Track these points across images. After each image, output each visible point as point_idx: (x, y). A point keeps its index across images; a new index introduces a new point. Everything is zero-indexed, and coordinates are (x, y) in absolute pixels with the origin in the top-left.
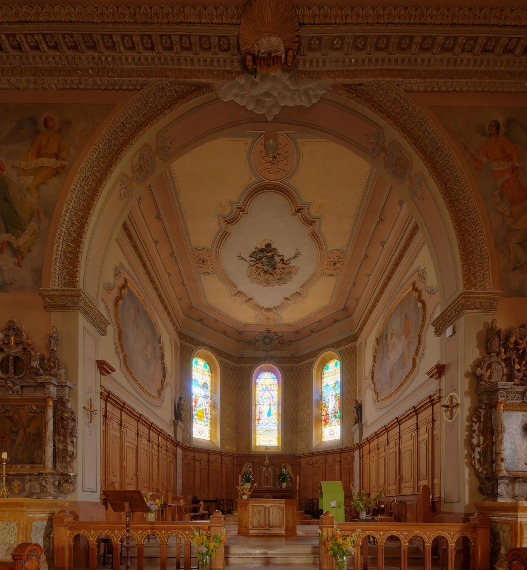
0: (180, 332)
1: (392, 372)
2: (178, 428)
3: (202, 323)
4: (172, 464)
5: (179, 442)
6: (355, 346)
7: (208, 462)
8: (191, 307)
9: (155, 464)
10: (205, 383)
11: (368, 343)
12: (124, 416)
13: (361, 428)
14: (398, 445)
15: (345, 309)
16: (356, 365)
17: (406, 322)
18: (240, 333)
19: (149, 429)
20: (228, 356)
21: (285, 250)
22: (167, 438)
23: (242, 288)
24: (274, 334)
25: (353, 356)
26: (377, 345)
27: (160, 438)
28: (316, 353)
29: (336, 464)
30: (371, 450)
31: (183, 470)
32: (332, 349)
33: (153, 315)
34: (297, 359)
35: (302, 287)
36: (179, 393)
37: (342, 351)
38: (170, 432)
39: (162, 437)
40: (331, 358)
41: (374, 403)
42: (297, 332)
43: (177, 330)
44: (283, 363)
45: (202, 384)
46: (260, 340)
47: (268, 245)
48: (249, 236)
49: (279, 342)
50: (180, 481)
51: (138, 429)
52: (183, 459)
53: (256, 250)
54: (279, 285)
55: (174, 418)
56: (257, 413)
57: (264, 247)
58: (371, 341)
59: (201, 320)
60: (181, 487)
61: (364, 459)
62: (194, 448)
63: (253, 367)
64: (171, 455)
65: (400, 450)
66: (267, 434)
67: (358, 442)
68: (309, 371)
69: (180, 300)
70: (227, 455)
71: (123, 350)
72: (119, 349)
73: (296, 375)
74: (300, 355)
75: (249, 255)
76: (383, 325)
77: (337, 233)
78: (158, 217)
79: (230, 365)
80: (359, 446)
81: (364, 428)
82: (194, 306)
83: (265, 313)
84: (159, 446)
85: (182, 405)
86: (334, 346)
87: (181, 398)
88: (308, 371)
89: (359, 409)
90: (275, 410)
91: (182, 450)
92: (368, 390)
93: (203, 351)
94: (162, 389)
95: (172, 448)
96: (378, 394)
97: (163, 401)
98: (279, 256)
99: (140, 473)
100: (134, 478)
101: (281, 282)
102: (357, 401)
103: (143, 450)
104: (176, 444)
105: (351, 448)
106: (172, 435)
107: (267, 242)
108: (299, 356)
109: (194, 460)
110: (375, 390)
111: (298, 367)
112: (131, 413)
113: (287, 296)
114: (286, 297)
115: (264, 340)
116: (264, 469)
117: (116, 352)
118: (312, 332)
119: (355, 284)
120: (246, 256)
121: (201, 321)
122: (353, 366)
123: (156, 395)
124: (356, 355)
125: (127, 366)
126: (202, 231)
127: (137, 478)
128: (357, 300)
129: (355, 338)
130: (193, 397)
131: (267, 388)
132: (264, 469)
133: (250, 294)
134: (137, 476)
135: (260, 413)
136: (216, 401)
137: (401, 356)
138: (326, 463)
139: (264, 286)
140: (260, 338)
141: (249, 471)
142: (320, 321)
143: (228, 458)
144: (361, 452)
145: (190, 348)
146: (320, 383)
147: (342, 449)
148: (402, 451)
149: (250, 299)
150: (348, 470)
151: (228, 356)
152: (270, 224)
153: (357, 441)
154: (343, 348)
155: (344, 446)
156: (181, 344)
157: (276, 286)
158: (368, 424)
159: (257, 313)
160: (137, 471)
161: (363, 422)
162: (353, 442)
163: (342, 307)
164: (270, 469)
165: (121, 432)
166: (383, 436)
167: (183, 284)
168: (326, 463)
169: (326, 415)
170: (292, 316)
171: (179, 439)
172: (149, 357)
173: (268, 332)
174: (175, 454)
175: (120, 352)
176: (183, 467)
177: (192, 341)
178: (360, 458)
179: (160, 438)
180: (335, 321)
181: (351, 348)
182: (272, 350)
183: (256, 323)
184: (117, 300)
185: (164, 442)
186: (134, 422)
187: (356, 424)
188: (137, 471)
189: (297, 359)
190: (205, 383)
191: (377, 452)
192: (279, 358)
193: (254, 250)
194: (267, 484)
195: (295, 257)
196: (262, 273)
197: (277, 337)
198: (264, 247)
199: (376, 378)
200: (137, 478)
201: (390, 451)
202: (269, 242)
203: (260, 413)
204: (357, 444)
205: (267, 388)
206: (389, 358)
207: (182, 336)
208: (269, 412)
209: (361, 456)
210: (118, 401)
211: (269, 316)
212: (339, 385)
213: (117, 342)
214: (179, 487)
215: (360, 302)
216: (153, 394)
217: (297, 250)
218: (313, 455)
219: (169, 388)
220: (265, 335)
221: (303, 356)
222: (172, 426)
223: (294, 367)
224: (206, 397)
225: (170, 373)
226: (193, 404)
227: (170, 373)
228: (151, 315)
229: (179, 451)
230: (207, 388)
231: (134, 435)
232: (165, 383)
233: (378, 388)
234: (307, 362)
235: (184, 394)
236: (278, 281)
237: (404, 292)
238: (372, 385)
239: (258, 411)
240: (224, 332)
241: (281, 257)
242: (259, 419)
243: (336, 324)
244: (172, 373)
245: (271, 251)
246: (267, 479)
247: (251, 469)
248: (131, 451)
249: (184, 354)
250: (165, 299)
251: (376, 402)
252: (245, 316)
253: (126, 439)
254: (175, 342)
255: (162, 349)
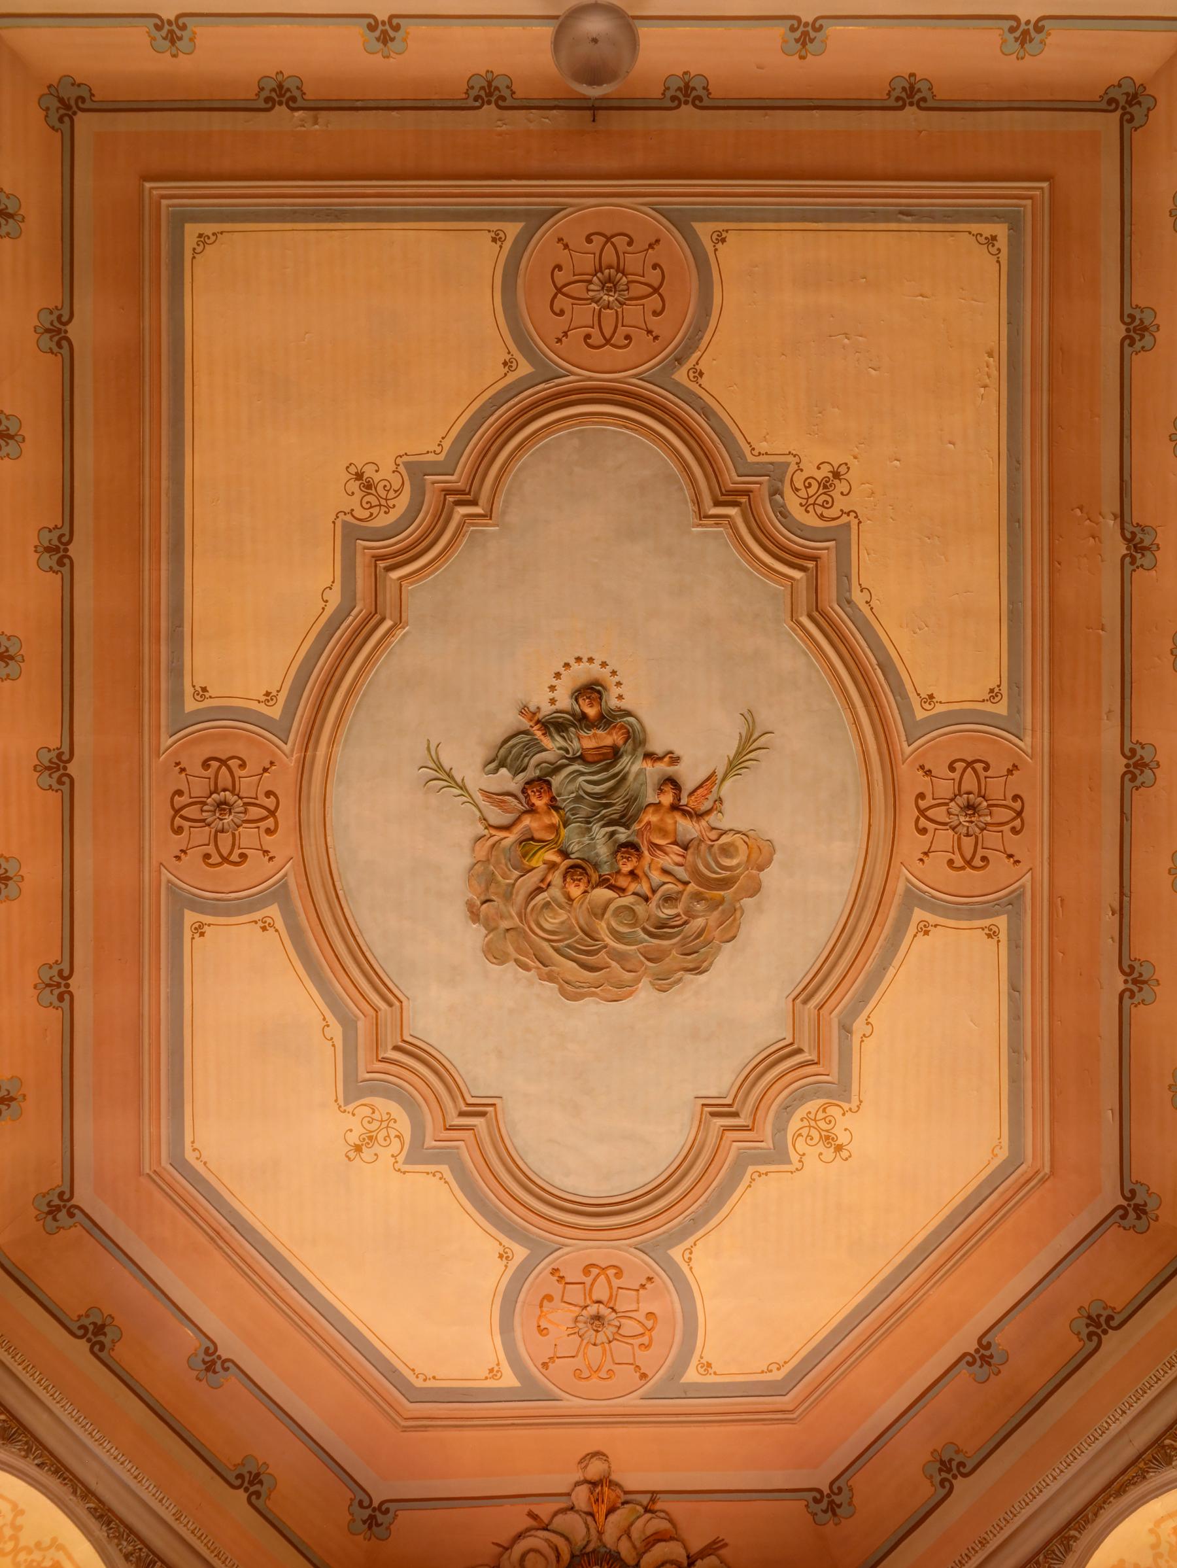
8: (60, 1207)
21: (687, 728)
24: (645, 1526)
47: (591, 690)
48: (486, 656)
53: (526, 724)
57: (564, 701)
75: (479, 759)
77: (943, 612)
78: (58, 552)
98: (649, 756)
107: (582, 673)
113: (719, 1082)
120: (467, 761)
126: (247, 626)
142: (983, 1355)
152: (596, 591)
180: (1099, 1325)
193: (510, 720)
195: (735, 765)
196: (556, 877)
198: (564, 701)
202: (595, 671)
217: (749, 718)
240: (251, 1482)
241: (663, 767)
243: (1111, 1340)
245: (606, 720)
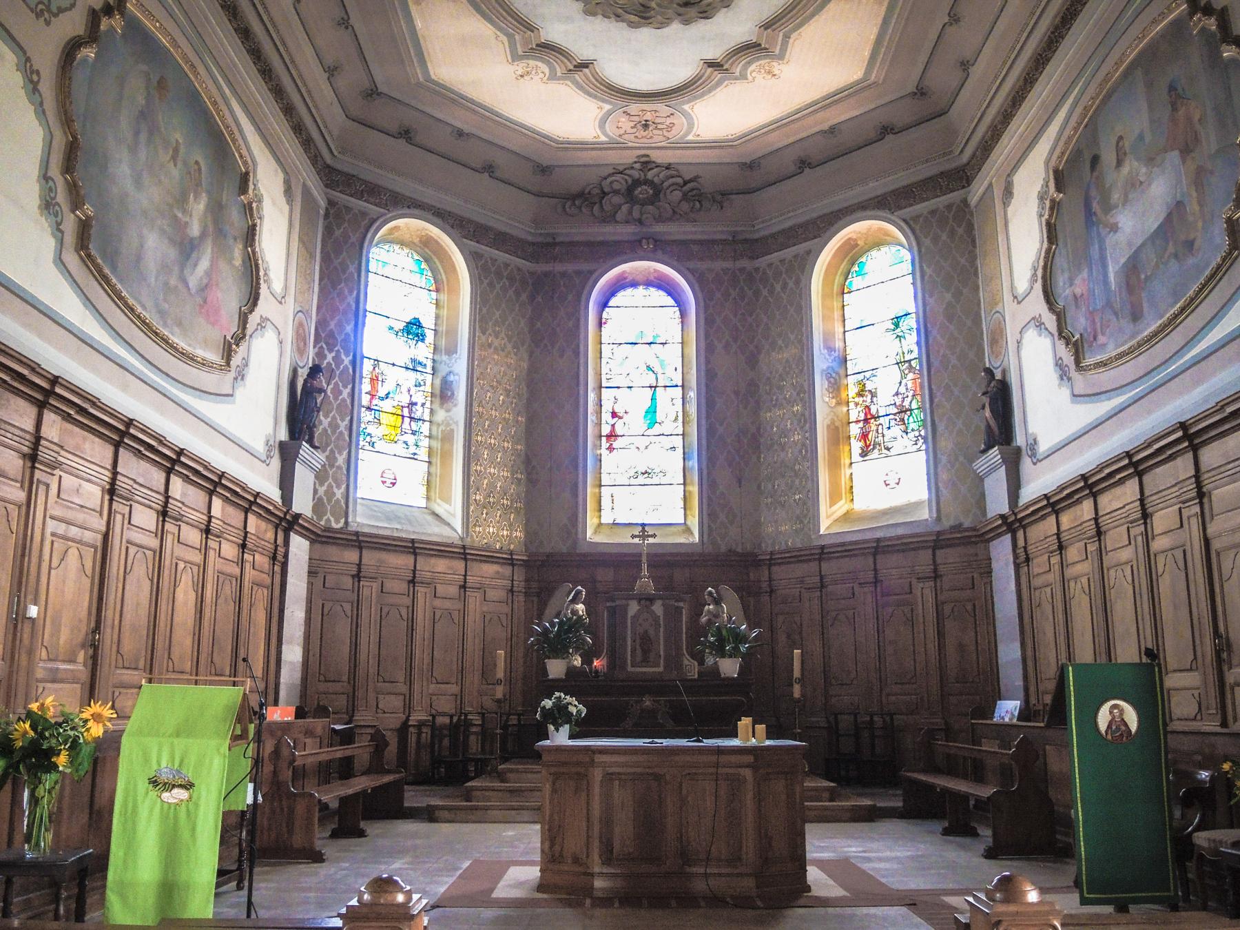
0: (328, 166)
1: (1132, 268)
2: (299, 469)
3: (409, 140)
4: (262, 595)
5: (298, 516)
6: (965, 202)
7: (412, 582)
8: (372, 93)
9: (185, 596)
10: (416, 323)
11: (1017, 190)
12: (53, 427)
13: (1013, 463)
14: (1195, 524)
15: (921, 92)
16: (973, 259)
17: (1175, 109)
18: (544, 170)
19: (169, 472)
20: (501, 240)
22: (249, 502)
23: (554, 32)
25: (960, 231)
26: (1059, 189)
27: (217, 503)
28: (823, 226)
29: (918, 587)
30: (1065, 537)
31: (309, 611)
32: (880, 213)
33: (223, 107)
34: (753, 247)
35: (767, 25)
36: (311, 352)
37: (916, 218)
38: (265, 482)
39: (226, 500)
40: (878, 243)
41: (1064, 375)
42: (751, 166)
43: (316, 160)
44: (701, 259)
45: (401, 325)
46: (616, 192)
49: (685, 197)
50: (293, 654)
51: (115, 473)
52: (312, 573)
54: (687, 22)
55: (283, 435)
56: (606, 416)
58: (1030, 183)
59: (407, 132)
60: (298, 675)
61: (1036, 570)
62: (357, 534)
63: (591, 272)
64: (262, 560)
65: (1207, 542)
66: (643, 486)
67: (1005, 509)
68: (798, 282)
69: (332, 71)
70: (488, 556)
71: (76, 202)
72: (61, 197)
73: (750, 293)
74: (763, 233)
76: (1076, 129)
79: (507, 265)
80: (1013, 524)
81: (1026, 463)
82: (382, 88)
83: (634, 108)
84: (207, 531)
85: (321, 390)
86: (882, 204)
87: (315, 370)
88: (791, 284)
89: (1001, 398)
90: (670, 404)
91: (312, 542)
92: (1031, 335)
93: (411, 225)
94: (240, 337)
95: (270, 535)
96: (1078, 350)
97: (241, 376)
99: (108, 636)
100: (81, 657)
101: (692, 12)
102: (989, 372)
103: (132, 550)
104: (288, 523)
105: (974, 529)
106: (274, 493)
108: (756, 236)
109: (358, 576)
110: (1062, 333)
111: (757, 269)
112: (86, 413)
113: (715, 53)
114: (710, 55)
115: (630, 190)
116: (634, 607)
117: (48, 205)
118: (804, 164)
119: (954, 18)
121: (406, 134)
122: (963, 261)
123: (214, 357)
124: (970, 227)
125: (89, 256)
127: (94, 658)
128: (965, 65)
129: (962, 176)
130: (367, 366)
131: (642, 337)
132: (634, 607)
133: (583, 51)
134: (95, 647)
135: (614, 415)
136: (451, 378)
137: (1169, 218)
138: (876, 581)
139: (632, 25)
140: (616, 186)
141: (574, 612)
143: (490, 569)
144: (1021, 543)
145: (364, 214)
146: (315, 648)
147: (939, 533)
148: (1216, 545)
149: (584, 65)
150: (969, 607)
151: (501, 240)
153: (998, 504)
154: (921, 208)
155: (947, 523)
156: (331, 203)
157: (675, 27)
158: (1043, 447)
159: (607, 107)
160: (97, 628)
161: (1020, 440)
162: (984, 512)
163: (911, 88)
164: (658, 608)
165: (30, 485)
166: (1118, 491)
167: (345, 23)
168: (876, 581)
169: (866, 421)
170: (726, 117)
171: (302, 504)
172: (195, 230)
173: (647, 164)
174: (280, 560)
175: (65, 207)
176: (309, 601)
177: (371, 191)
178: (1017, 567)
179: (217, 503)
181: (949, 207)
182: (659, 219)
183: (603, 139)
184: (71, 48)
185: (235, 516)
186: (99, 451)
187: (989, 447)
188: (97, 628)
189: (753, 247)
190: (416, 323)
191: (1092, 548)
192: (684, 243)
194: (645, 661)
197: (679, 180)
199: (1064, 291)
200: (94, 658)
201: (1158, 544)
203: (614, 415)
204: (1002, 517)
205: (642, 337)
206: (1114, 228)
207: (331, 176)
208: (652, 411)
209: (1022, 560)
210: (25, 372)
211: (648, 116)
212: (911, 322)
213: (55, 172)
214: (290, 674)
215: (977, 71)
216: (200, 353)
218: (823, 553)
219: (270, 334)
220: (636, 174)
221: (773, 236)
222: (276, 463)
223: (742, 270)
224: (415, 366)
225: (278, 286)
226: (366, 386)
227: (278, 286)
228: (215, 103)
229: (299, 547)
230: (421, 337)
231: (93, 494)
232: (253, 319)
233: (1079, 323)
234: (788, 253)
235: (330, 357)
236: (682, 10)
237: (1155, 22)
238: (1050, 320)
239: (607, 407)
240: (489, 169)
242: (612, 436)
244: (286, 287)
246: (646, 643)
247: (580, 607)
248: (73, 553)
249: (338, 233)
250: (286, 81)
251: (1074, 374)
252: (566, 117)
253: (57, 512)
254: (306, 192)
255: (248, 210)
